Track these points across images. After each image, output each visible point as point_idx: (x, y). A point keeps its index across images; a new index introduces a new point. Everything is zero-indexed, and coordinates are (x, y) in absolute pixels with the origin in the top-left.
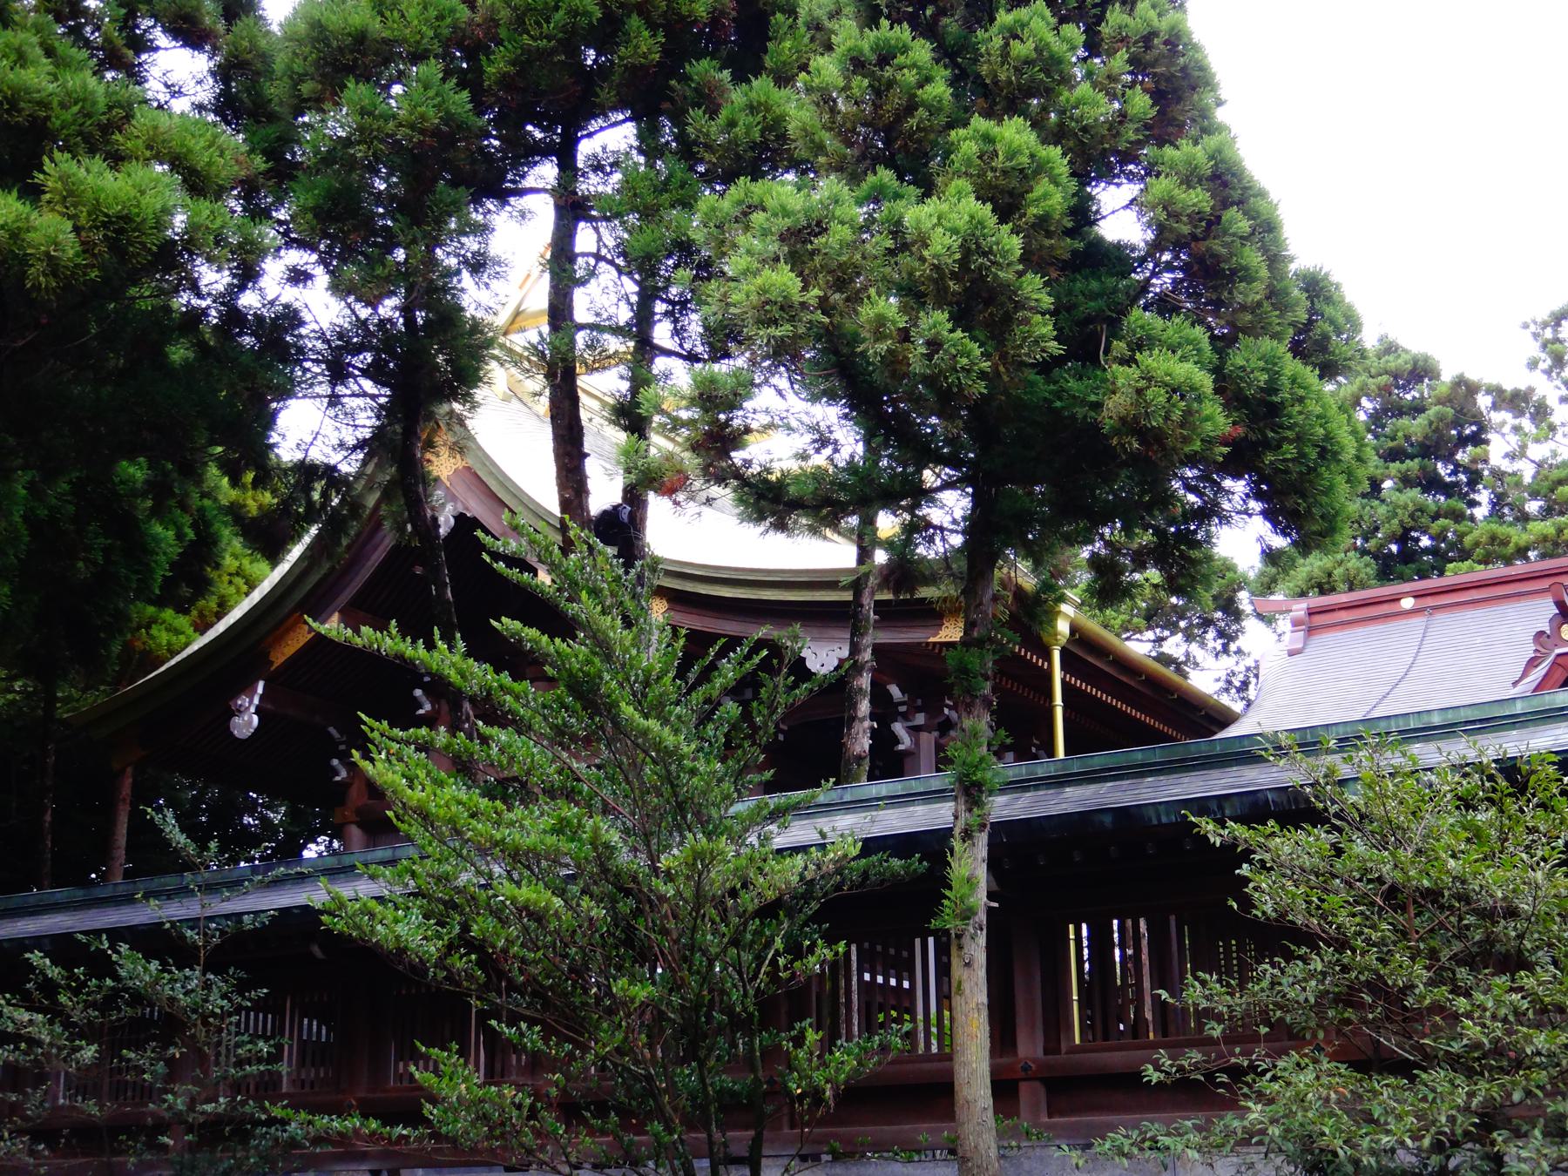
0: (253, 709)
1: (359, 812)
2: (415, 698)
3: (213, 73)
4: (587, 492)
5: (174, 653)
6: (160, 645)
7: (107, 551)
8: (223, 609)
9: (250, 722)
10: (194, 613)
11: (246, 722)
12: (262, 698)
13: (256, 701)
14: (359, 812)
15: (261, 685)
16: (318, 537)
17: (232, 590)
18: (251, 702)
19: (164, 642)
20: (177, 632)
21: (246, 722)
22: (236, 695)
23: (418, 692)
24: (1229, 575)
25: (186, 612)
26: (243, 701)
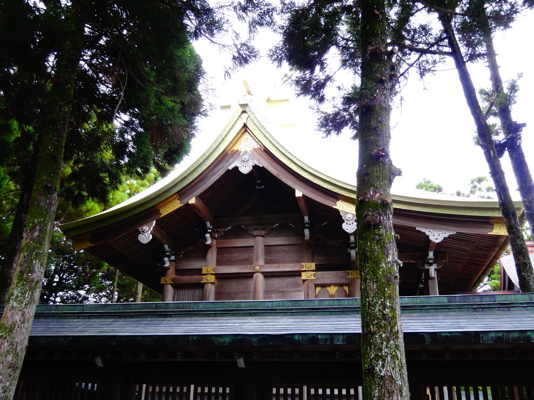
0: (150, 232)
1: (173, 280)
13: (152, 229)
15: (155, 222)
16: (156, 224)
18: (149, 229)
22: (143, 225)
26: (145, 228)
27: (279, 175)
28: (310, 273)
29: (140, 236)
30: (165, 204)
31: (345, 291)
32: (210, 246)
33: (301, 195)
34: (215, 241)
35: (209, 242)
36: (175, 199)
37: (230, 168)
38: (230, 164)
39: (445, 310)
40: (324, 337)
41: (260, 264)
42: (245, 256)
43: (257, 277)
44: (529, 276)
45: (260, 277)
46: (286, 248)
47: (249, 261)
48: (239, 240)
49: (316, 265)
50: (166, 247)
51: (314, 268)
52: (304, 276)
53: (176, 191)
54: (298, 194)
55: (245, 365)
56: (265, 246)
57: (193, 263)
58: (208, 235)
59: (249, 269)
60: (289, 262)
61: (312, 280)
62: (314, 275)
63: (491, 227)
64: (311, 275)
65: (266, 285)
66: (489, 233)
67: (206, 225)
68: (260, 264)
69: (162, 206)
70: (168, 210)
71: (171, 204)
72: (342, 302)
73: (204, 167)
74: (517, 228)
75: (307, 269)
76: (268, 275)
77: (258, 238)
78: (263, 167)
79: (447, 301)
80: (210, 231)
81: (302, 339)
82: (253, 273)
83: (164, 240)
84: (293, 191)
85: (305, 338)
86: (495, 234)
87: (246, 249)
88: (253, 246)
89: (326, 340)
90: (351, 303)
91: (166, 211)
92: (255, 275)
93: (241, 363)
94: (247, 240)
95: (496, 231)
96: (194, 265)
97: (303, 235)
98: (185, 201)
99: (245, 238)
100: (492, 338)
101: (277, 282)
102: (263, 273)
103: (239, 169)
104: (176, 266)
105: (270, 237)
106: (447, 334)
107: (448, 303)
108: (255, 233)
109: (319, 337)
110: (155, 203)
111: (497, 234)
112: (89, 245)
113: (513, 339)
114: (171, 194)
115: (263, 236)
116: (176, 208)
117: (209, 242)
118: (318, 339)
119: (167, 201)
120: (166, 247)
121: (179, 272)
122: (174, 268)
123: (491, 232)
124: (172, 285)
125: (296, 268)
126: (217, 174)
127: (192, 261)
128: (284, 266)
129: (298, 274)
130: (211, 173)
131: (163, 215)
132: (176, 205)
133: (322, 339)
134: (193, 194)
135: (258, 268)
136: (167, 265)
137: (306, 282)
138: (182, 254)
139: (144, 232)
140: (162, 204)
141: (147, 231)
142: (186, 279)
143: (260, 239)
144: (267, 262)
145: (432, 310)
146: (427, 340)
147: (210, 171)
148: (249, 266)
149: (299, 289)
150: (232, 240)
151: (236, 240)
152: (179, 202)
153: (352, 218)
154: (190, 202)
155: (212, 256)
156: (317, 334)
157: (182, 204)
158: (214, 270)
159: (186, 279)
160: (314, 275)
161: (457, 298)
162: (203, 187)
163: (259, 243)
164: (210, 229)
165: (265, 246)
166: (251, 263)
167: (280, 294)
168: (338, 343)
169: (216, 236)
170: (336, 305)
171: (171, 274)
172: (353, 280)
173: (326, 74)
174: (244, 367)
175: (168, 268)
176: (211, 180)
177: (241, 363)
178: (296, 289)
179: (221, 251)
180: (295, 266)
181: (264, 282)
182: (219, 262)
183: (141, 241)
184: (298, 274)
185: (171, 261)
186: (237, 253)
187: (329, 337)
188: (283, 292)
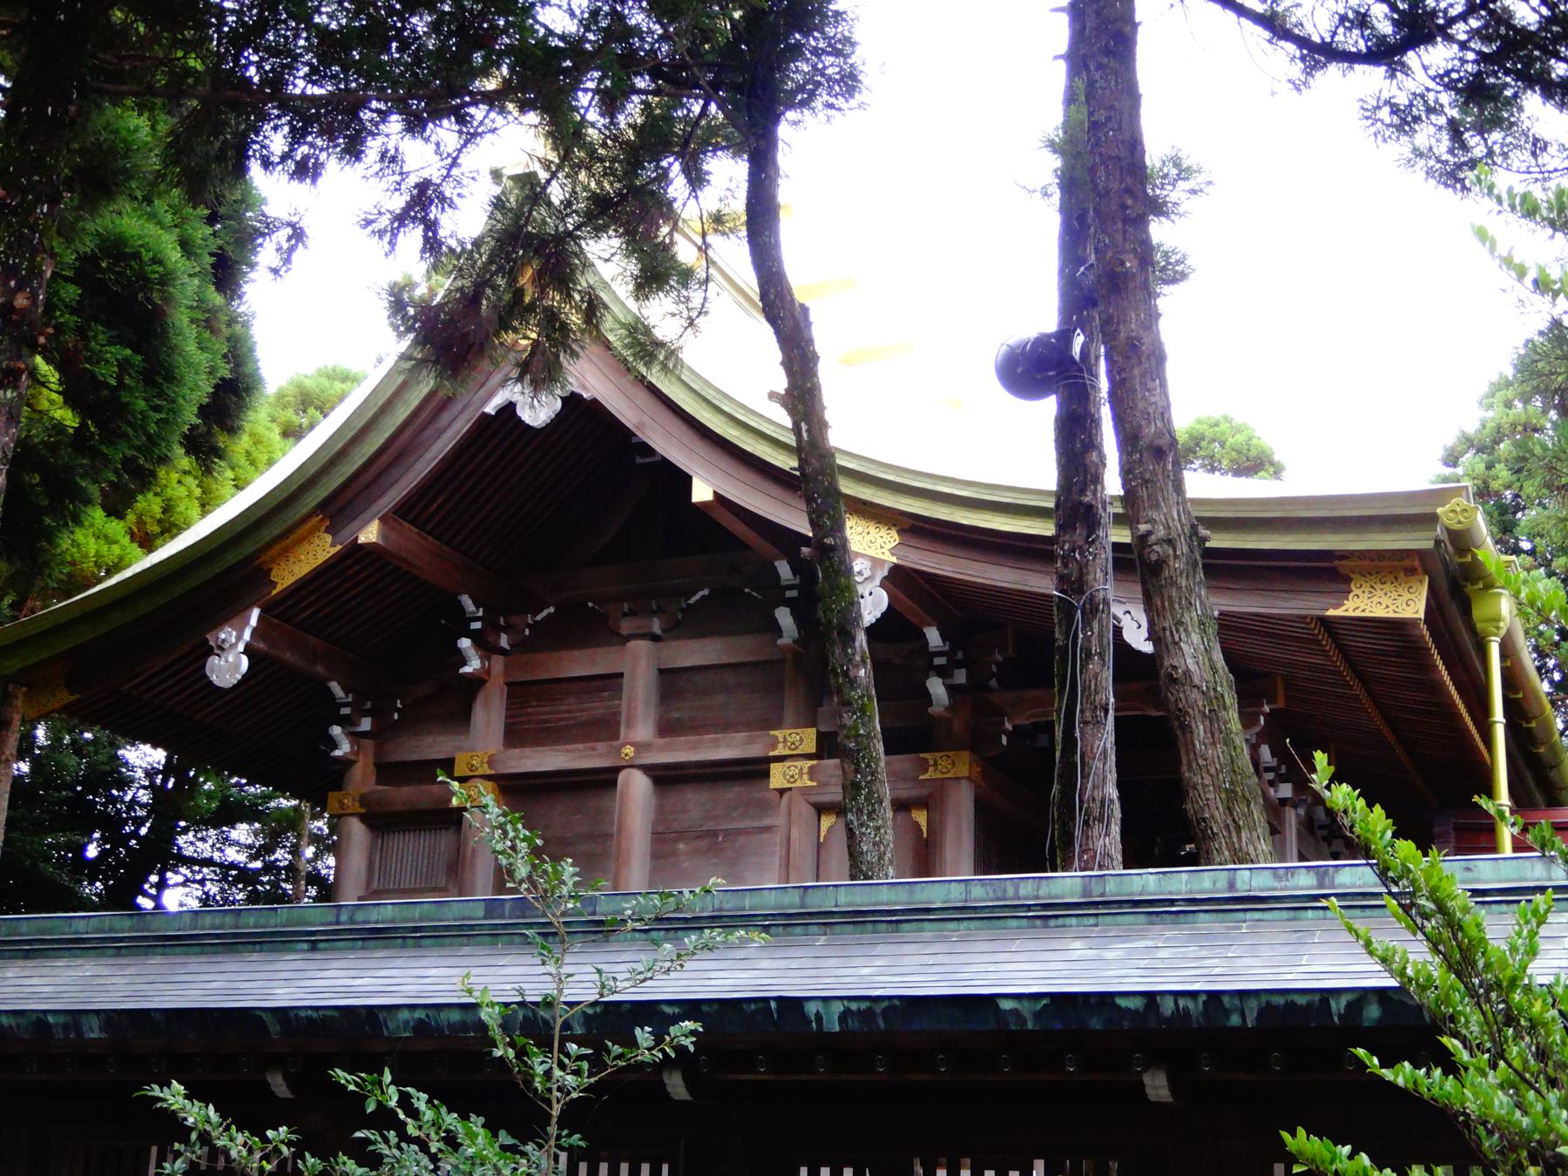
0: (241, 647)
1: (364, 800)
2: (459, 650)
3: (353, 151)
4: (783, 363)
5: (110, 572)
6: (86, 556)
7: (123, 365)
8: (170, 528)
9: (238, 665)
10: (131, 517)
11: (229, 664)
12: (255, 632)
13: (247, 636)
14: (364, 800)
15: (255, 614)
16: (260, 618)
17: (182, 491)
18: (239, 638)
19: (92, 553)
20: (110, 541)
21: (229, 664)
22: (218, 624)
23: (465, 643)
24: (238, 327)
25: (120, 516)
26: (227, 634)
27: (641, 426)
28: (799, 764)
29: (214, 661)
30: (287, 551)
31: (917, 825)
32: (476, 684)
33: (709, 497)
34: (498, 663)
35: (473, 665)
36: (312, 532)
37: (490, 408)
38: (491, 395)
39: (458, 940)
40: (61, 1019)
41: (641, 736)
42: (596, 707)
43: (627, 784)
44: (862, 825)
45: (637, 786)
46: (730, 678)
47: (607, 728)
48: (577, 653)
49: (819, 733)
50: (335, 687)
51: (810, 746)
52: (778, 776)
53: (312, 504)
54: (701, 492)
55: (689, 1088)
56: (662, 671)
57: (430, 739)
58: (465, 643)
59: (601, 755)
60: (728, 727)
61: (805, 791)
62: (812, 773)
63: (1344, 587)
64: (801, 773)
65: (661, 812)
66: (1331, 612)
67: (462, 609)
68: (641, 736)
69: (279, 555)
70: (296, 568)
71: (306, 545)
72: (245, 919)
73: (401, 414)
74: (846, 674)
75: (789, 752)
76: (666, 778)
77: (633, 643)
78: (595, 401)
79: (481, 913)
80: (477, 625)
81: (18, 1025)
82: (616, 770)
83: (319, 669)
84: (685, 481)
85: (23, 1021)
86: (1350, 614)
87: (600, 683)
88: (621, 675)
89: (66, 1027)
90: (262, 921)
91: (290, 572)
92: (622, 776)
93: (1157, 1086)
94: (602, 651)
95: (1358, 602)
96: (433, 746)
97: (776, 629)
98: (346, 535)
99: (598, 645)
100: (406, 1023)
101: (694, 803)
102: (647, 769)
103: (519, 412)
104: (379, 751)
105: (678, 638)
106: (329, 1013)
107: (485, 918)
108: (626, 626)
109: (51, 1019)
110: (248, 548)
111: (1358, 614)
112: (66, 698)
113: (451, 1026)
114: (298, 517)
115: (655, 638)
116: (320, 561)
117: (473, 665)
118: (48, 1024)
119: (289, 539)
120: (335, 687)
121: (388, 772)
122: (371, 760)
123: (1337, 606)
124: (363, 818)
125: (755, 751)
126: (449, 434)
127: (430, 733)
128: (716, 744)
129: (755, 770)
130: (428, 432)
131: (279, 588)
132: (320, 550)
133: (57, 1024)
134: (374, 508)
135: (629, 750)
136: (344, 749)
137: (786, 796)
138: (398, 710)
139: (222, 649)
140: (278, 548)
141: (234, 646)
142: (404, 795)
143: (641, 647)
144: (667, 728)
145: (428, 942)
146: (271, 1029)
147: (424, 428)
148: (601, 746)
149: (767, 822)
150: (555, 655)
151: (565, 654)
152: (329, 538)
153: (867, 573)
154: (362, 539)
155: (489, 717)
156: (45, 1012)
157: (339, 547)
158: (490, 763)
159: (404, 795)
160: (812, 773)
161: (508, 906)
162: (402, 484)
163: (637, 664)
164: (477, 619)
165: (662, 671)
166: (615, 735)
167: (704, 844)
168: (92, 1036)
169: (504, 641)
170: (228, 925)
171: (362, 779)
172: (941, 785)
173: (413, 180)
174: (289, 1095)
175: (346, 764)
176: (428, 455)
177: (1157, 1086)
178: (756, 824)
179: (520, 694)
180: (750, 741)
181: (653, 801)
182: (515, 735)
183: (214, 678)
184: (755, 770)
185: (356, 737)
186: (571, 700)
187: (69, 1018)
188: (715, 833)
